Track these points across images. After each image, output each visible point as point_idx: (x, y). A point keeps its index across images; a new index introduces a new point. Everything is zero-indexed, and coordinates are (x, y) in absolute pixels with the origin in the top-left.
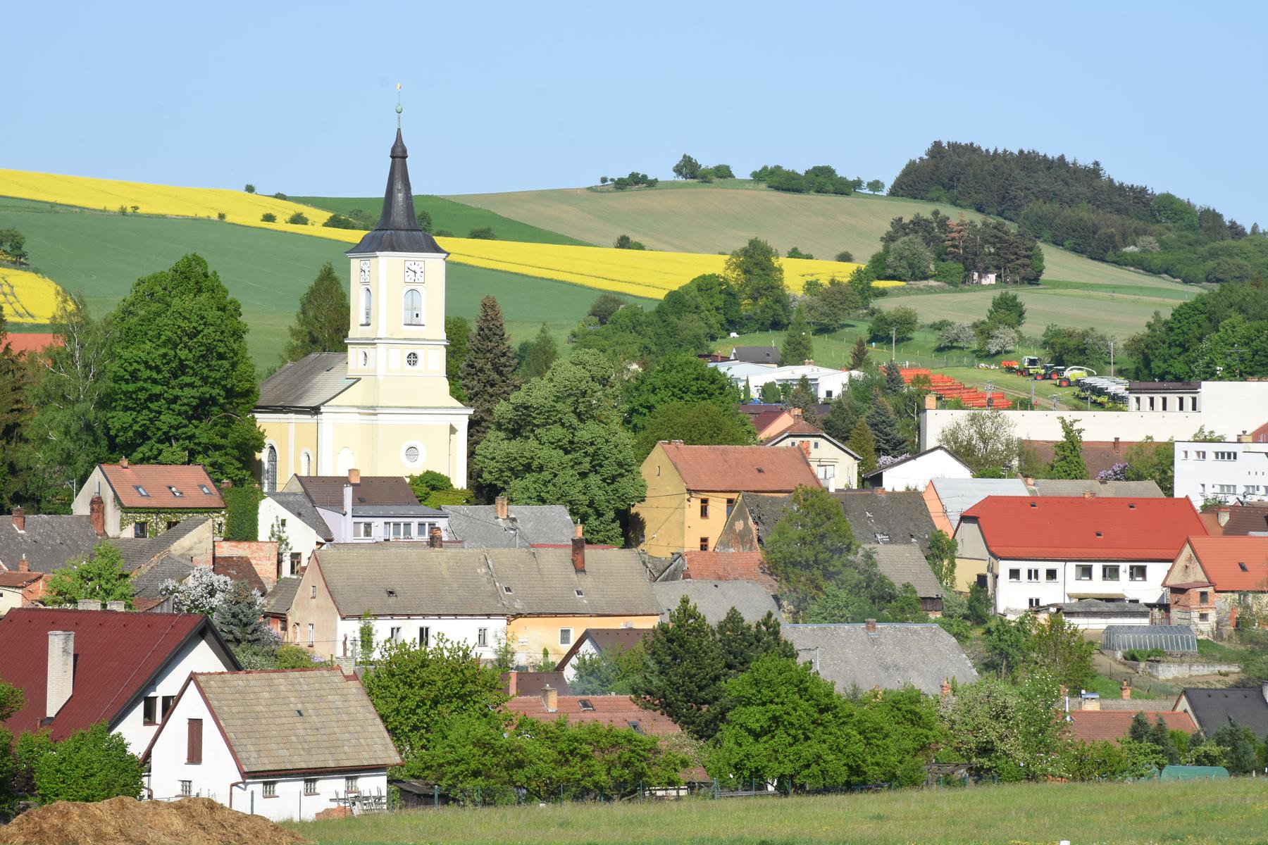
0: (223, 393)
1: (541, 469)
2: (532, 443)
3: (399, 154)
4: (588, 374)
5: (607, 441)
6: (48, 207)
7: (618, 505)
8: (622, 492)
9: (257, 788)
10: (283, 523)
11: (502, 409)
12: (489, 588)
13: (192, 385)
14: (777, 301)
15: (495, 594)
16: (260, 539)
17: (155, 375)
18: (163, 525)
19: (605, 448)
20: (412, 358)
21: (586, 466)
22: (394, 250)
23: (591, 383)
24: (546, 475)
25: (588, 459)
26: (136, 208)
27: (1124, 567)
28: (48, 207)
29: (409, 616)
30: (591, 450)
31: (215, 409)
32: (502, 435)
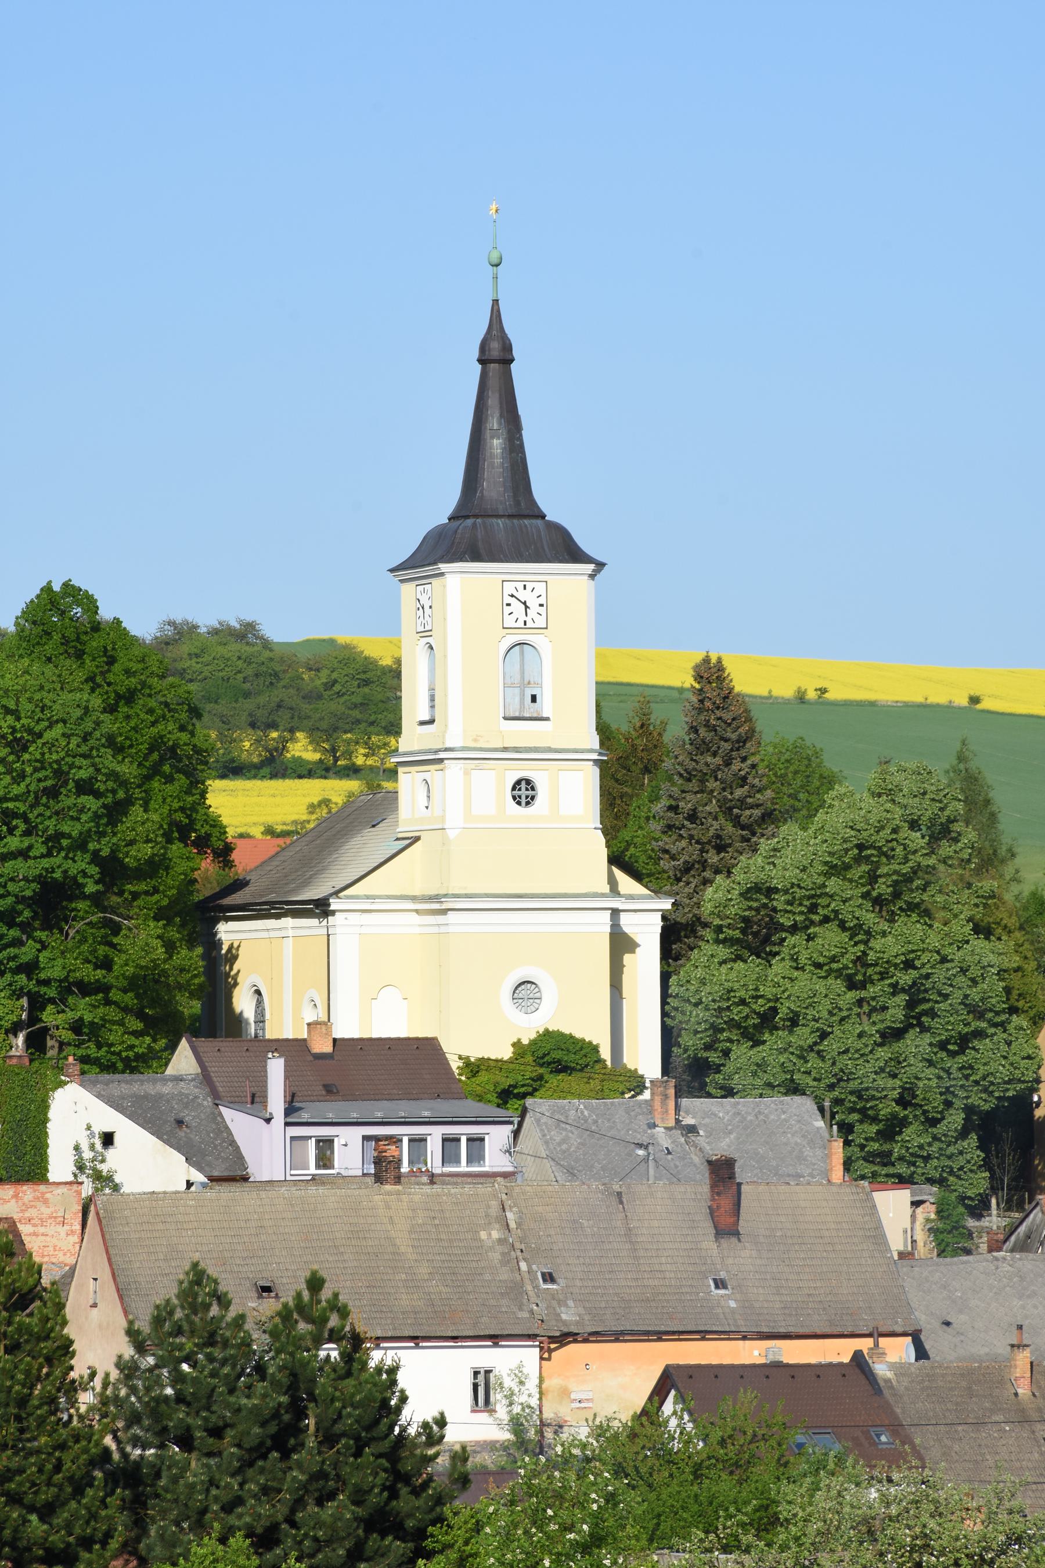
0: (94, 870)
1: (794, 1021)
2: (779, 967)
3: (496, 356)
4: (898, 812)
5: (944, 960)
6: (676, 694)
7: (975, 1100)
8: (982, 1070)
10: (108, 1139)
11: (719, 896)
12: (504, 1274)
13: (23, 854)
15: (515, 1291)
16: (52, 1177)
19: (940, 975)
20: (524, 791)
21: (896, 1011)
22: (476, 557)
23: (905, 832)
24: (803, 1036)
25: (902, 999)
26: (823, 691)
28: (676, 694)
30: (906, 978)
31: (82, 905)
32: (723, 952)
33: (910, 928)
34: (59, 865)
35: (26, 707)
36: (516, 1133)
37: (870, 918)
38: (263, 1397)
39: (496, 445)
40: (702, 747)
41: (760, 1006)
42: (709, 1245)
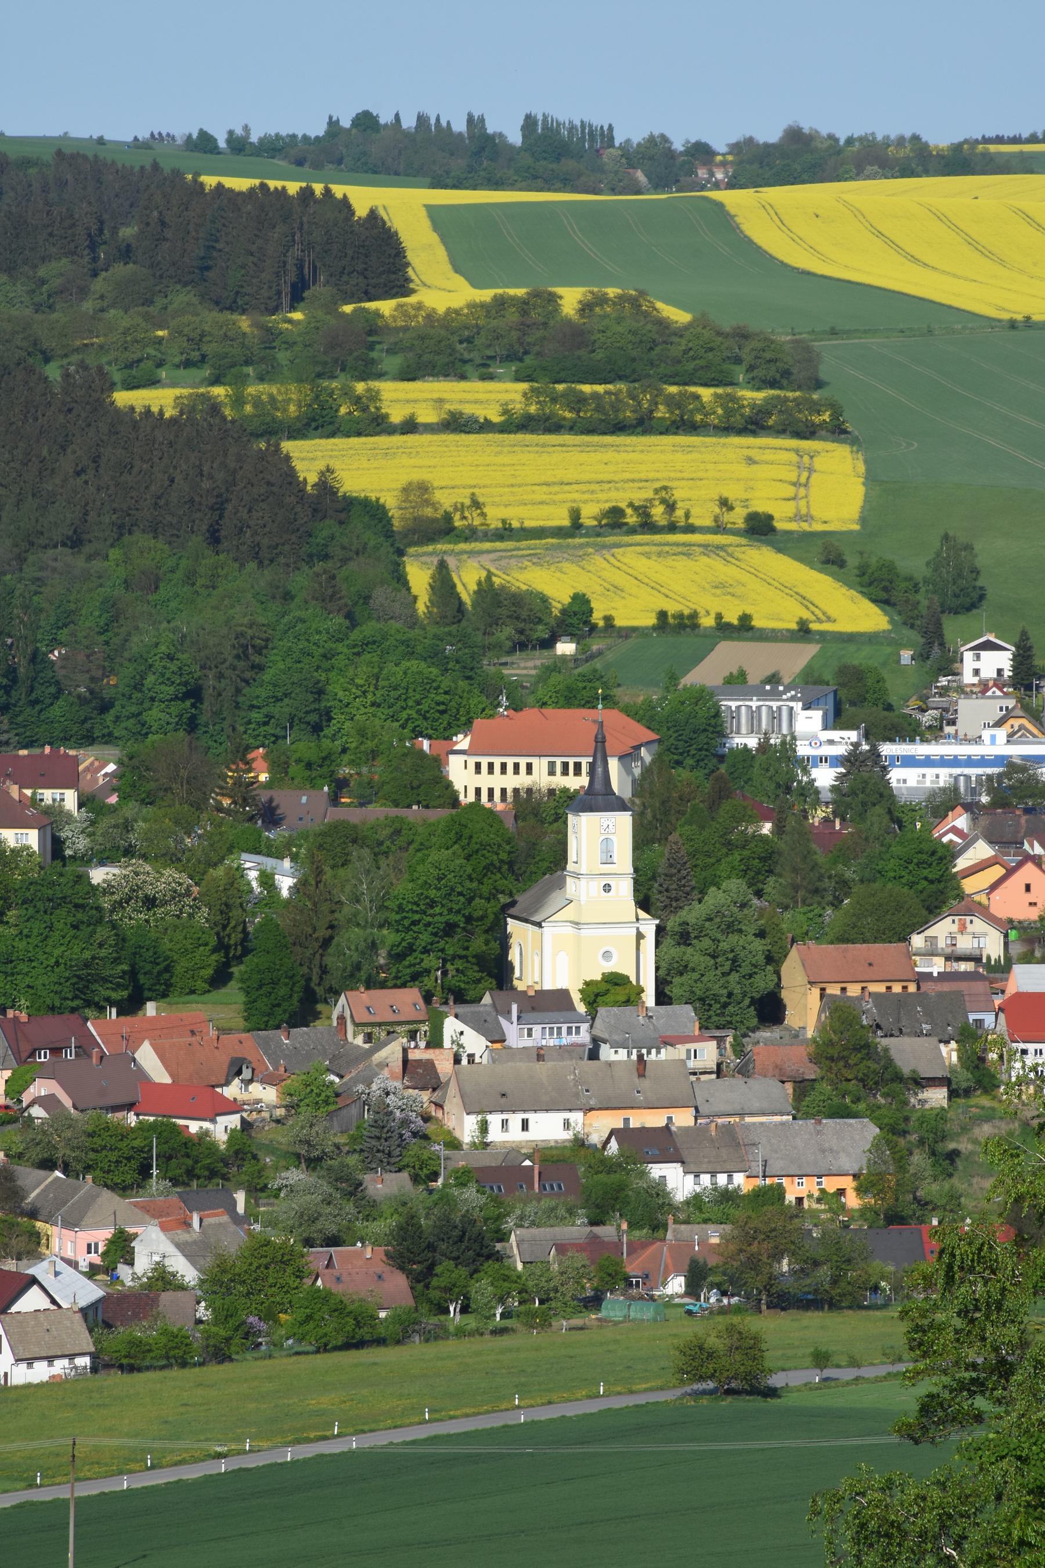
9: (23, 1366)
10: (462, 1033)
13: (441, 914)
17: (415, 908)
18: (383, 1034)
19: (742, 954)
20: (607, 888)
22: (592, 810)
29: (514, 1112)
30: (731, 956)
33: (734, 938)
35: (443, 866)
36: (591, 1027)
37: (719, 936)
38: (456, 1233)
39: (600, 770)
40: (671, 866)
41: (683, 963)
42: (636, 1079)
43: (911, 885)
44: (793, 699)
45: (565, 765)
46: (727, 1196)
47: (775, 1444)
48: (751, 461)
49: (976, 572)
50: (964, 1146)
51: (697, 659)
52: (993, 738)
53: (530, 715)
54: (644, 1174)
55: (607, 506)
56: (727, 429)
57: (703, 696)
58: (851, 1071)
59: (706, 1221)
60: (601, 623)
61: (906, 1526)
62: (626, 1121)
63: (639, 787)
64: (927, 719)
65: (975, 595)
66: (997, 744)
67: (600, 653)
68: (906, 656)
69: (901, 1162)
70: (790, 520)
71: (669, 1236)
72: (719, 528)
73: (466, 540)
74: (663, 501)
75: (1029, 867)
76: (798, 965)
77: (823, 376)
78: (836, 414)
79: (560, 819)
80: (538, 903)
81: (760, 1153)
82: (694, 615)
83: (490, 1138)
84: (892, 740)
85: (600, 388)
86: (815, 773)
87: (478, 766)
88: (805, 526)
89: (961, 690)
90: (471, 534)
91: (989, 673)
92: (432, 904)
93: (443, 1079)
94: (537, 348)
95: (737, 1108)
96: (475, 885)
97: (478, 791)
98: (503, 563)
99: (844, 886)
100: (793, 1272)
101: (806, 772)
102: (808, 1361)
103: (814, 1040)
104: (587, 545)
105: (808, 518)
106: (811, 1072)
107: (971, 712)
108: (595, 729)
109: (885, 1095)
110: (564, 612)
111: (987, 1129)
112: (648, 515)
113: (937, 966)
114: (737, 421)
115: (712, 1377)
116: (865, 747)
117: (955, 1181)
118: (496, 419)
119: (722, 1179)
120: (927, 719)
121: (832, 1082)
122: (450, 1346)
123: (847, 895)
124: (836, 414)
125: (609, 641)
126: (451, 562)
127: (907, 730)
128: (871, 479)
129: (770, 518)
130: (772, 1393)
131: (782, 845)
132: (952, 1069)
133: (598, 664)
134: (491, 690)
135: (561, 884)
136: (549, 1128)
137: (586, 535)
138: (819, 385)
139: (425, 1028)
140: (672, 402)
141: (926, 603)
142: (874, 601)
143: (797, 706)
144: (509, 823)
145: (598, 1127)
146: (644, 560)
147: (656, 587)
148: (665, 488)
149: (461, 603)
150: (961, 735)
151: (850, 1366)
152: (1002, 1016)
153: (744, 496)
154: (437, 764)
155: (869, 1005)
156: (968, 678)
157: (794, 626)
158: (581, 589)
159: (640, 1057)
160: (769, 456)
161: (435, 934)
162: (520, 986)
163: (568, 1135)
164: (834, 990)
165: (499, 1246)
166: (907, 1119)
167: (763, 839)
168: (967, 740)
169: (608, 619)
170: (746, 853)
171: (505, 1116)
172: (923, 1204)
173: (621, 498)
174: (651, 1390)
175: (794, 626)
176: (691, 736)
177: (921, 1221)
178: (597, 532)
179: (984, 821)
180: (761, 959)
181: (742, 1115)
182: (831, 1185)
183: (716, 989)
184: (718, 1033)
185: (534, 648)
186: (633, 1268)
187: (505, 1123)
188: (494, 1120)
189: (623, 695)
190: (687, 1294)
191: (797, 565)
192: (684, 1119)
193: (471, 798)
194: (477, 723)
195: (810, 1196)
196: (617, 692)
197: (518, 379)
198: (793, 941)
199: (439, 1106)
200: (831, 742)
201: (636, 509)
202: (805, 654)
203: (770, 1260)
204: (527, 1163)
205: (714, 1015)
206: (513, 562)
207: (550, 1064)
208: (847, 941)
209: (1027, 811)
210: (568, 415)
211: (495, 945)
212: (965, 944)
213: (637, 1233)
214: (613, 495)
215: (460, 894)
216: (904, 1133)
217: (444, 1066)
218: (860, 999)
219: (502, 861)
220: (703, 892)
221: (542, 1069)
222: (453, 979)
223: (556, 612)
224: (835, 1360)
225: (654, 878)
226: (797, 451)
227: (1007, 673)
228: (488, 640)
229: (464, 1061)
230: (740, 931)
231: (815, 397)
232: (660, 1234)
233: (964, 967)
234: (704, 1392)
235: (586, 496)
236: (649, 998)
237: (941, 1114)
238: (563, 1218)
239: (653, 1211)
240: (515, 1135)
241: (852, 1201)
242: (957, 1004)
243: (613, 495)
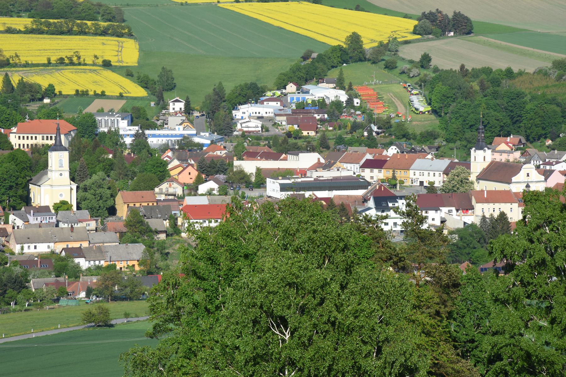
14: (361, 52)
15: (52, 238)
20: (61, 175)
22: (56, 151)
27: (213, 220)
33: (101, 190)
34: (12, 184)
37: (96, 189)
38: (13, 280)
39: (58, 138)
43: (155, 173)
44: (118, 117)
45: (47, 137)
46: (99, 268)
47: (113, 341)
48: (103, 44)
49: (173, 79)
50: (171, 251)
51: (89, 104)
52: (179, 128)
53: (36, 121)
54: (73, 262)
55: (59, 57)
56: (96, 34)
57: (91, 116)
58: (137, 229)
59: (92, 275)
60: (58, 93)
61: (148, 362)
62: (67, 245)
63: (71, 144)
64: (159, 123)
65: (173, 86)
66: (180, 131)
67: (58, 102)
68: (152, 104)
69: (152, 256)
70: (116, 62)
71: (81, 280)
72: (94, 64)
73: (14, 67)
74: (76, 56)
75: (190, 167)
76: (121, 197)
77: (125, 18)
78: (129, 31)
79: (46, 153)
80: (39, 179)
81: (109, 254)
82: (87, 91)
83: (24, 251)
84: (149, 129)
85: (56, 21)
86: (125, 139)
87: (19, 137)
88: (121, 64)
89: (169, 114)
90: (15, 65)
91: (177, 109)
92: (5, 180)
93: (9, 234)
94: (35, 8)
95: (102, 241)
96: (19, 174)
97: (19, 145)
98: (26, 74)
99: (134, 173)
100: (118, 290)
101: (122, 139)
102: (123, 316)
103: (125, 220)
104: (53, 69)
105: (122, 62)
106: (125, 230)
107: (173, 121)
108: (56, 126)
109: (147, 236)
110: (46, 90)
111: (178, 246)
112: (72, 60)
113: (163, 197)
114: (99, 31)
115: (93, 322)
116: (141, 131)
117: (168, 261)
118: (23, 30)
119: (97, 263)
120: (159, 123)
121: (131, 233)
122: (11, 315)
123: (135, 176)
124: (130, 30)
125: (60, 99)
126: (9, 74)
127: (153, 127)
128: (141, 50)
129: (110, 61)
130: (112, 326)
131: (115, 161)
132: (167, 228)
133: (57, 106)
134: (23, 114)
135: (46, 174)
136: (43, 248)
137: (53, 66)
138: (124, 21)
139: (3, 218)
140: (78, 25)
141: (158, 88)
142: (142, 87)
143: (120, 119)
144: (30, 155)
145: (59, 247)
146: (71, 74)
147: (75, 82)
148: (77, 52)
149: (13, 87)
150: (169, 128)
151: (133, 318)
152: (182, 212)
153: (102, 55)
154: (6, 136)
155: (142, 209)
156: (171, 111)
157: (118, 95)
158: (51, 83)
159: (72, 226)
160: (109, 42)
161: (6, 189)
162: (34, 205)
163: (49, 250)
164: (131, 205)
165: (27, 284)
166: (154, 243)
167: (110, 159)
168: (171, 129)
169: (60, 92)
170: (104, 164)
171: (29, 245)
172: (158, 268)
173: (63, 55)
174: (74, 326)
175: (118, 95)
176: (87, 128)
177: (158, 273)
178: (56, 65)
179: (176, 154)
180: (109, 196)
181: (103, 243)
182: (130, 263)
183: (95, 205)
184: (96, 218)
185: (37, 101)
186: (69, 290)
187: (29, 247)
188: (26, 246)
189: (65, 115)
190: (86, 297)
191: (119, 76)
192: (85, 244)
193: (17, 147)
194: (19, 124)
195: (124, 267)
196: (63, 114)
197: (29, 17)
198: (119, 190)
199: (8, 242)
200: (130, 130)
201: (68, 58)
202: (122, 103)
203: (113, 287)
204: (36, 259)
205: (95, 213)
206: (29, 74)
207: (43, 229)
208: (136, 190)
209: (189, 150)
210: (46, 29)
211: (25, 192)
212: (171, 191)
213: (70, 279)
214: (61, 54)
215: (14, 176)
216: (153, 247)
217: (9, 229)
218: (139, 207)
219: (27, 167)
220: (91, 176)
221: (41, 230)
222: (12, 203)
223: (43, 90)
224: (131, 315)
225: (76, 171)
226: (118, 41)
227: (183, 109)
228: (22, 98)
229: (16, 228)
230: (103, 187)
231: (123, 24)
232: (78, 279)
233: (171, 197)
234: (91, 326)
235: (52, 54)
236: (74, 208)
237: (164, 242)
238: (47, 275)
239: (76, 273)
240: (32, 250)
241: (137, 268)
242: (169, 208)
243: (61, 54)
